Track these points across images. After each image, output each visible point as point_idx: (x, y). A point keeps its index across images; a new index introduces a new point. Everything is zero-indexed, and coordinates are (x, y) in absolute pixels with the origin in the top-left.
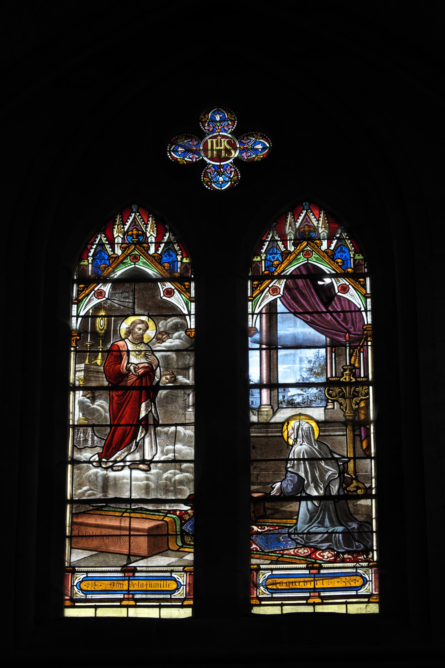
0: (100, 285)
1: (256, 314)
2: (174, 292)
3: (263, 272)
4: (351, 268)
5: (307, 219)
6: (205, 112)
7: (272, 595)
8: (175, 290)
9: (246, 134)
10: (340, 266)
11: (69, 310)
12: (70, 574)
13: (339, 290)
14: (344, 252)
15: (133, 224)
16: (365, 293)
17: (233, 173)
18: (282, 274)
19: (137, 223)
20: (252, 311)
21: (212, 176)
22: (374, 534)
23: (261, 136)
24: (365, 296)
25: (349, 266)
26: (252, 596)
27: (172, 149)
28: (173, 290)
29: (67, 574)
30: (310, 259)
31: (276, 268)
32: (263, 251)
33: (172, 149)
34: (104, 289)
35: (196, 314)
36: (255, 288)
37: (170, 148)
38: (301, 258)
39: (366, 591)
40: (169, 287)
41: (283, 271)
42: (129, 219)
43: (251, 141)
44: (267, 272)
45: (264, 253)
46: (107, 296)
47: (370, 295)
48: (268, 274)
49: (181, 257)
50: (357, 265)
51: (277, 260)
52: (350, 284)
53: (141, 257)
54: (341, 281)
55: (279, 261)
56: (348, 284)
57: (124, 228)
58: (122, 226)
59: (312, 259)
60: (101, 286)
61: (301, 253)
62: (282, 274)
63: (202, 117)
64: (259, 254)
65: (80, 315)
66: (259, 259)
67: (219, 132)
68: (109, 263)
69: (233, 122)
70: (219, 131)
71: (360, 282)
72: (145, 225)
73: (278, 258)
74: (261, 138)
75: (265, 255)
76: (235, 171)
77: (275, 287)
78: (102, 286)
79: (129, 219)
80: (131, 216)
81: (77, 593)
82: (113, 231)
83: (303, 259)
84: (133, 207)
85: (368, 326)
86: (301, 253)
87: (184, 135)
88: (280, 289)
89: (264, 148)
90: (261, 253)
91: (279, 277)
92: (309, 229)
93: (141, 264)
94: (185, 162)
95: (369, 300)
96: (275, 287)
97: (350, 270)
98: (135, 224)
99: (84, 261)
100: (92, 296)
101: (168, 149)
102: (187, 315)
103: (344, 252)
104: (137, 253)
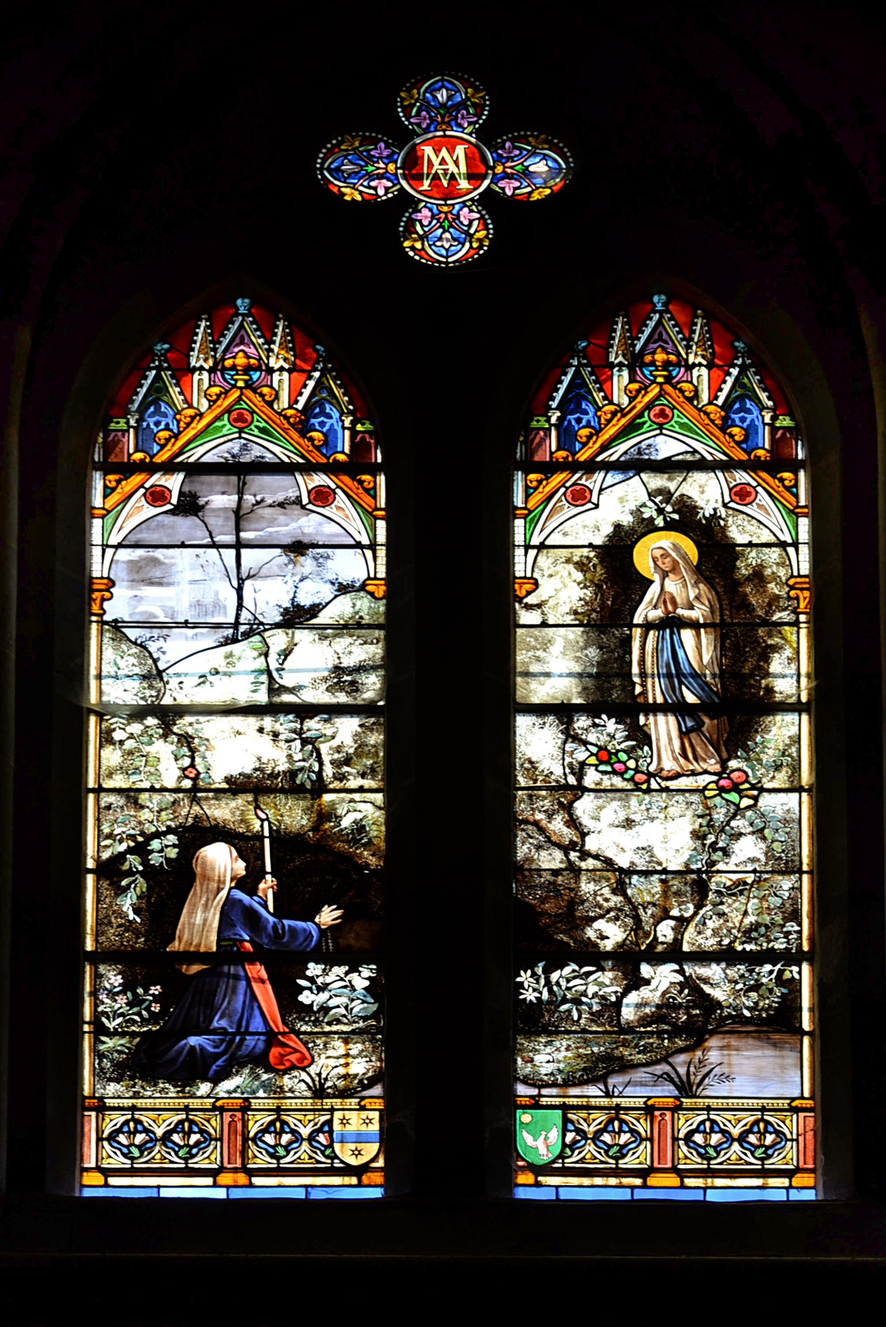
0: (577, 476)
1: (533, 547)
2: (335, 493)
3: (130, 455)
4: (343, 452)
5: (660, 334)
6: (412, 84)
7: (186, 1163)
8: (338, 491)
9: (510, 136)
10: (738, 444)
11: (509, 532)
12: (93, 1114)
13: (312, 498)
14: (749, 411)
15: (656, 336)
16: (373, 506)
17: (476, 223)
18: (599, 459)
19: (665, 336)
20: (525, 541)
21: (426, 229)
22: (806, 1040)
23: (546, 141)
24: (794, 513)
25: (339, 449)
26: (86, 1165)
27: (326, 165)
28: (334, 491)
29: (86, 1113)
30: (246, 430)
31: (163, 447)
32: (554, 404)
33: (326, 165)
34: (587, 484)
35: (389, 545)
36: (793, 486)
37: (322, 164)
38: (224, 426)
39: (637, 1161)
40: (322, 483)
41: (180, 452)
42: (229, 329)
43: (521, 153)
44: (139, 456)
45: (136, 411)
46: (174, 500)
47: (383, 513)
48: (142, 461)
49: (351, 418)
50: (359, 447)
51: (588, 425)
52: (338, 487)
53: (676, 411)
54: (737, 475)
55: (171, 430)
56: (754, 484)
57: (634, 346)
58: (211, 346)
59: (251, 430)
60: (580, 478)
61: (226, 416)
62: (599, 459)
63: (403, 94)
64: (125, 414)
65: (532, 544)
66: (122, 425)
67: (444, 131)
68: (178, 427)
69: (479, 109)
70: (444, 127)
71: (361, 482)
72: (685, 343)
73: (167, 424)
74: (546, 146)
75: (558, 414)
76: (482, 218)
77: (159, 489)
78: (584, 478)
79: (229, 329)
80: (651, 319)
81: (256, 1157)
82: (189, 356)
83: (651, 426)
84: (656, 299)
85: (799, 580)
86: (646, 414)
87: (358, 136)
88: (591, 491)
89: (554, 172)
90: (549, 408)
91: (169, 468)
92: (665, 357)
93: (677, 429)
94: (359, 198)
95: (381, 525)
96: (159, 489)
97: (760, 452)
98: (660, 338)
99: (118, 423)
100: (559, 500)
101: (318, 166)
102: (790, 545)
103: (749, 411)
104: (245, 406)
